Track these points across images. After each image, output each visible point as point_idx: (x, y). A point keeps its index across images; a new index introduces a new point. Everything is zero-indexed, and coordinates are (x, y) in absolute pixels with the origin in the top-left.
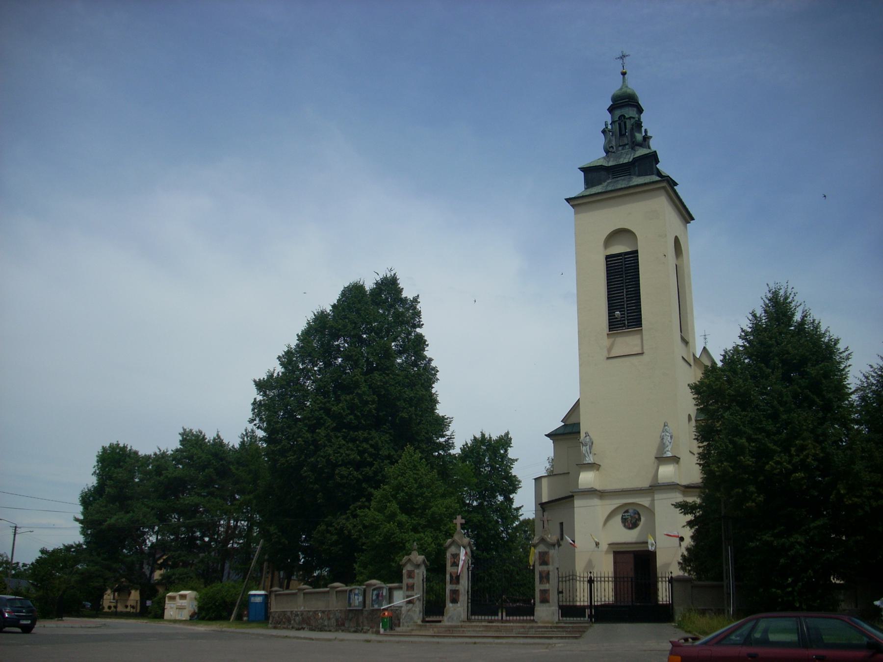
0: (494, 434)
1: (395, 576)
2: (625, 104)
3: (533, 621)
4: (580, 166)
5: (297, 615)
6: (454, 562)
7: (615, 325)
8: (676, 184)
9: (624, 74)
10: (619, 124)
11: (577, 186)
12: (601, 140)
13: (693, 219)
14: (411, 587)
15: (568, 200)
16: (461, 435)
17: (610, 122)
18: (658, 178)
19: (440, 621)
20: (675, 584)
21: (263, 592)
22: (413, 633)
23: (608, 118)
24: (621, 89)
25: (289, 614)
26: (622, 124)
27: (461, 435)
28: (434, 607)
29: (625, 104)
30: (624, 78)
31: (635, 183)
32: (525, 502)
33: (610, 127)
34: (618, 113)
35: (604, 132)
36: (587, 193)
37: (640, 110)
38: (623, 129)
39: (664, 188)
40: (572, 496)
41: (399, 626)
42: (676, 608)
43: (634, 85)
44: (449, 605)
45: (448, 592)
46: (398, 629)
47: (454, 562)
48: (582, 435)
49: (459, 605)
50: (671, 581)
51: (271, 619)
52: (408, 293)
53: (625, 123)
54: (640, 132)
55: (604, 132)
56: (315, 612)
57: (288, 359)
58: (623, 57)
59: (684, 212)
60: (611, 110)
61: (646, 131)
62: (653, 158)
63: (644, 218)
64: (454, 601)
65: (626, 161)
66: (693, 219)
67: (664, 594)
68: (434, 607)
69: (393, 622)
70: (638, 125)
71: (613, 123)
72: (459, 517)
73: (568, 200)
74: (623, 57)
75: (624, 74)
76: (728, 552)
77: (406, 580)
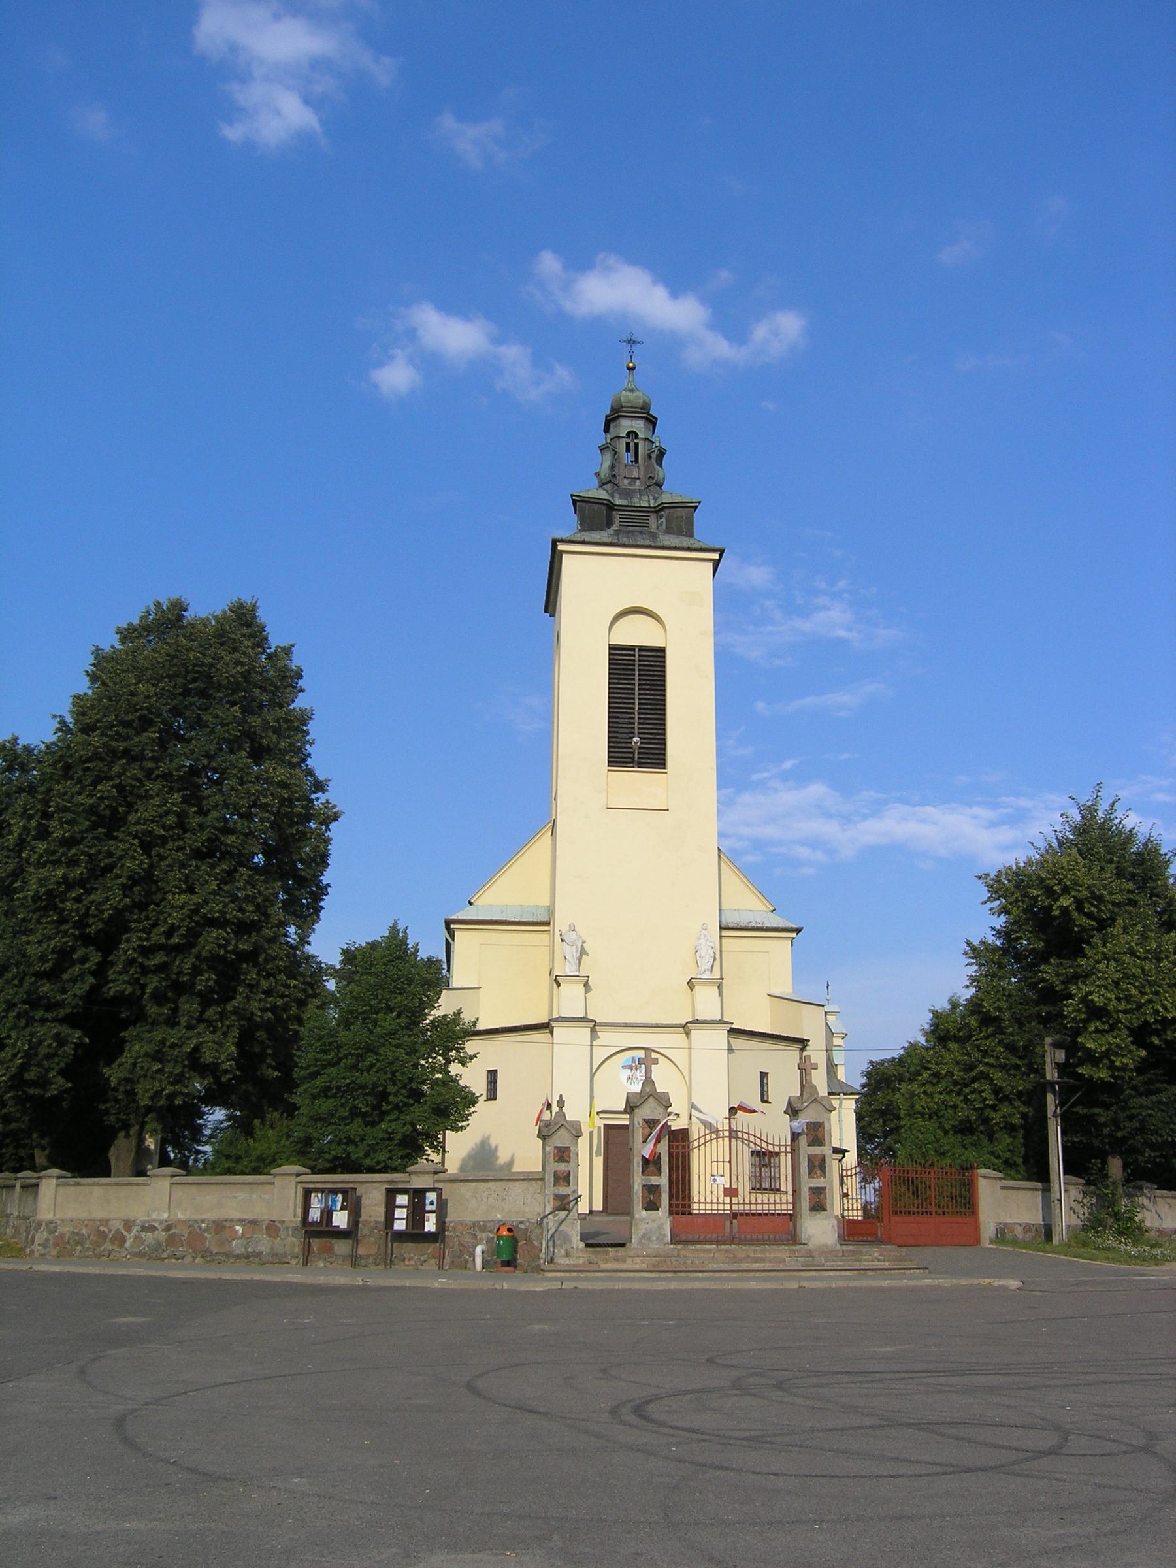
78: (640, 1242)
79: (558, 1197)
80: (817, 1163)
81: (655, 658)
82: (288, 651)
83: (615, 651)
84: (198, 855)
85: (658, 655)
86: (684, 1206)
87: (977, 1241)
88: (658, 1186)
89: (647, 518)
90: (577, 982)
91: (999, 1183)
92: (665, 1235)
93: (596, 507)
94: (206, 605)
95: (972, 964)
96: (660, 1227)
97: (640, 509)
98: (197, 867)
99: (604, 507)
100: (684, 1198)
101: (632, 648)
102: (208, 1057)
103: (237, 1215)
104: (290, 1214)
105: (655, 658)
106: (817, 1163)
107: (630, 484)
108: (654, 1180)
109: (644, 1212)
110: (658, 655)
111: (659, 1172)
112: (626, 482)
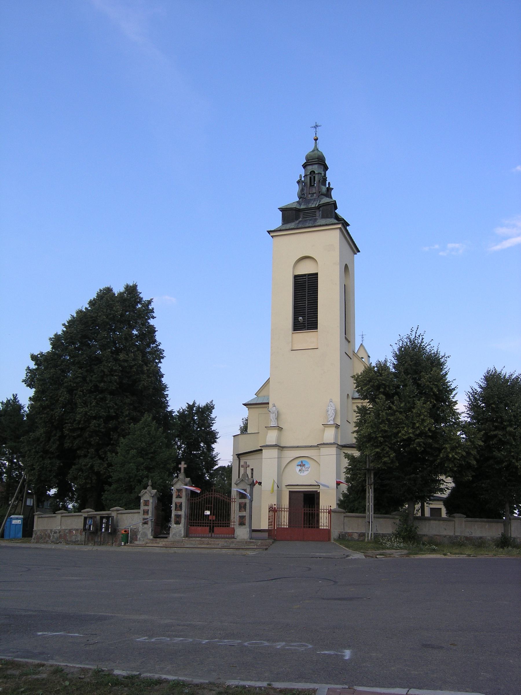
0: (202, 403)
1: (134, 504)
2: (316, 163)
3: (234, 538)
4: (280, 206)
5: (55, 533)
6: (179, 495)
7: (298, 327)
8: (348, 225)
9: (316, 140)
10: (310, 178)
11: (277, 221)
12: (296, 188)
13: (359, 251)
14: (146, 512)
15: (269, 232)
16: (176, 403)
17: (303, 175)
18: (336, 221)
19: (166, 538)
20: (332, 514)
21: (22, 516)
22: (147, 545)
23: (302, 172)
24: (313, 151)
25: (49, 531)
26: (312, 177)
27: (176, 403)
28: (162, 525)
29: (316, 163)
30: (316, 142)
31: (319, 224)
32: (224, 453)
33: (303, 179)
34: (310, 168)
35: (298, 182)
36: (284, 228)
37: (326, 168)
38: (313, 180)
39: (340, 228)
40: (261, 450)
41: (137, 540)
42: (332, 530)
43: (324, 150)
44: (173, 526)
45: (173, 515)
46: (136, 543)
47: (179, 495)
48: (271, 405)
49: (181, 525)
50: (330, 512)
51: (34, 536)
52: (145, 296)
53: (314, 177)
54: (325, 185)
55: (298, 182)
56: (70, 531)
57: (56, 341)
58: (316, 126)
59: (353, 247)
60: (305, 166)
61: (329, 183)
62: (334, 205)
63: (319, 246)
64: (178, 523)
65: (313, 206)
66: (359, 251)
67: (324, 521)
68: (162, 525)
69: (129, 537)
70: (325, 179)
71: (306, 176)
72: (183, 463)
73: (269, 232)
74: (316, 126)
75: (316, 140)
76: (370, 494)
77: (143, 507)
78: (173, 537)
79: (144, 519)
80: (242, 506)
81: (313, 278)
82: (150, 302)
83: (296, 277)
84: (90, 392)
85: (315, 276)
86: (228, 524)
87: (329, 539)
88: (180, 515)
89: (315, 212)
90: (275, 429)
91: (343, 515)
92: (181, 534)
93: (290, 212)
94: (118, 289)
95: (456, 409)
96: (180, 531)
97: (311, 209)
98: (89, 397)
99: (294, 212)
100: (228, 520)
101: (305, 275)
102: (96, 469)
103: (75, 527)
104: (81, 526)
105: (313, 278)
106: (242, 506)
107: (311, 197)
108: (179, 513)
109: (175, 525)
110: (315, 276)
111: (181, 510)
112: (309, 196)
